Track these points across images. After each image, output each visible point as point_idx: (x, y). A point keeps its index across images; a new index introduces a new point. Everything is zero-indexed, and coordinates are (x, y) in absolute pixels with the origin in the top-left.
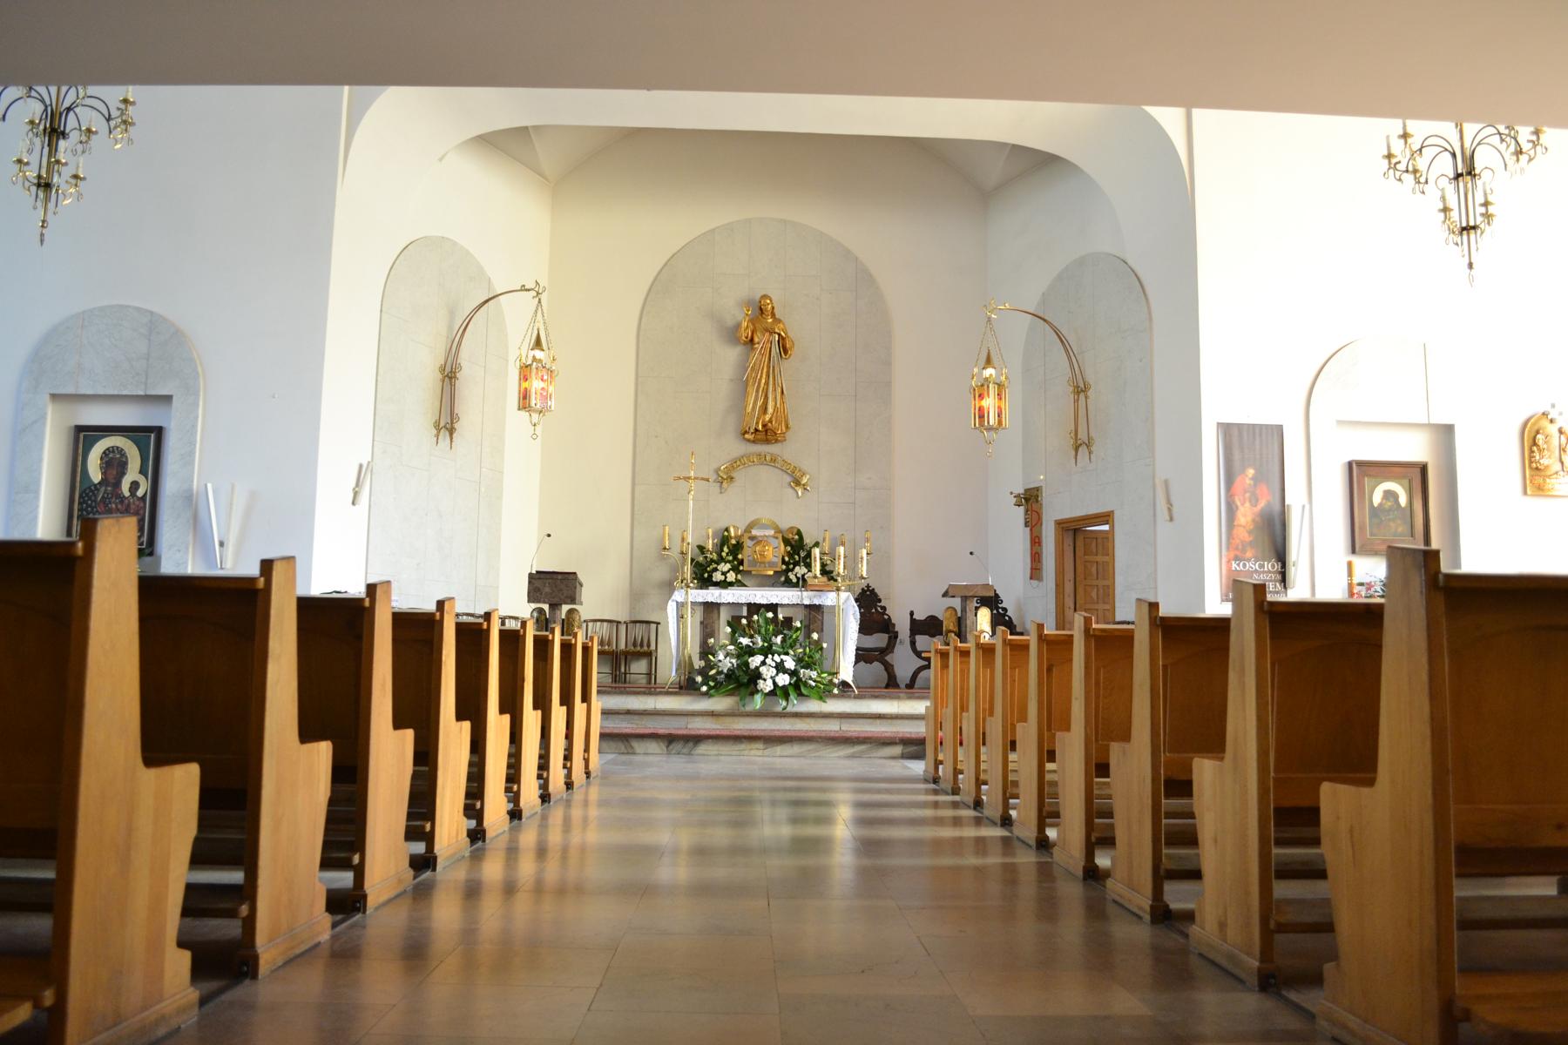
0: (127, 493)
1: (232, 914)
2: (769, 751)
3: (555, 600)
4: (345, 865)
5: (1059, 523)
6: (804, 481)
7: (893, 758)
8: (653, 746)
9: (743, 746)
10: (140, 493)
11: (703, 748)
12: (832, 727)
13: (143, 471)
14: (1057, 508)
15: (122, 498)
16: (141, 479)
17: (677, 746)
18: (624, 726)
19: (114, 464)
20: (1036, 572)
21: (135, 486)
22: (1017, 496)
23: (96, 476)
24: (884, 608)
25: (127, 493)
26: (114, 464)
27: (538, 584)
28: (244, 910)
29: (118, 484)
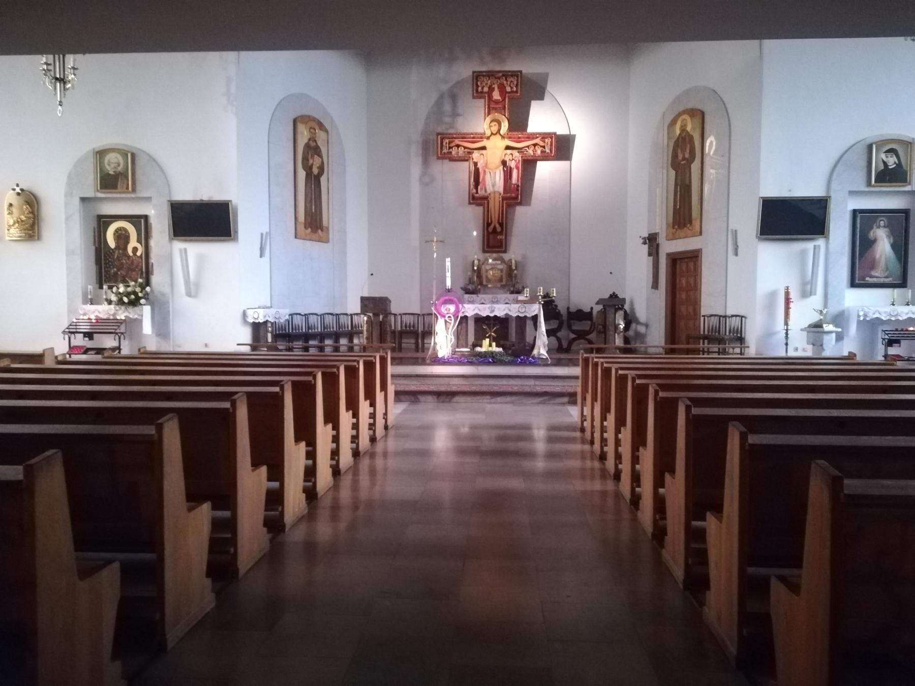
0: (131, 254)
1: (276, 510)
2: (493, 400)
3: (376, 312)
4: (310, 481)
5: (668, 255)
6: (69, 86)
7: (563, 404)
8: (430, 398)
9: (479, 397)
10: (139, 254)
11: (457, 399)
12: (540, 386)
13: (139, 241)
14: (668, 247)
15: (129, 257)
16: (138, 245)
17: (442, 398)
18: (413, 386)
19: (122, 237)
20: (655, 285)
21: (135, 250)
22: (644, 238)
23: (112, 244)
24: (556, 306)
25: (131, 254)
26: (122, 237)
27: (366, 302)
28: (280, 509)
29: (125, 249)
